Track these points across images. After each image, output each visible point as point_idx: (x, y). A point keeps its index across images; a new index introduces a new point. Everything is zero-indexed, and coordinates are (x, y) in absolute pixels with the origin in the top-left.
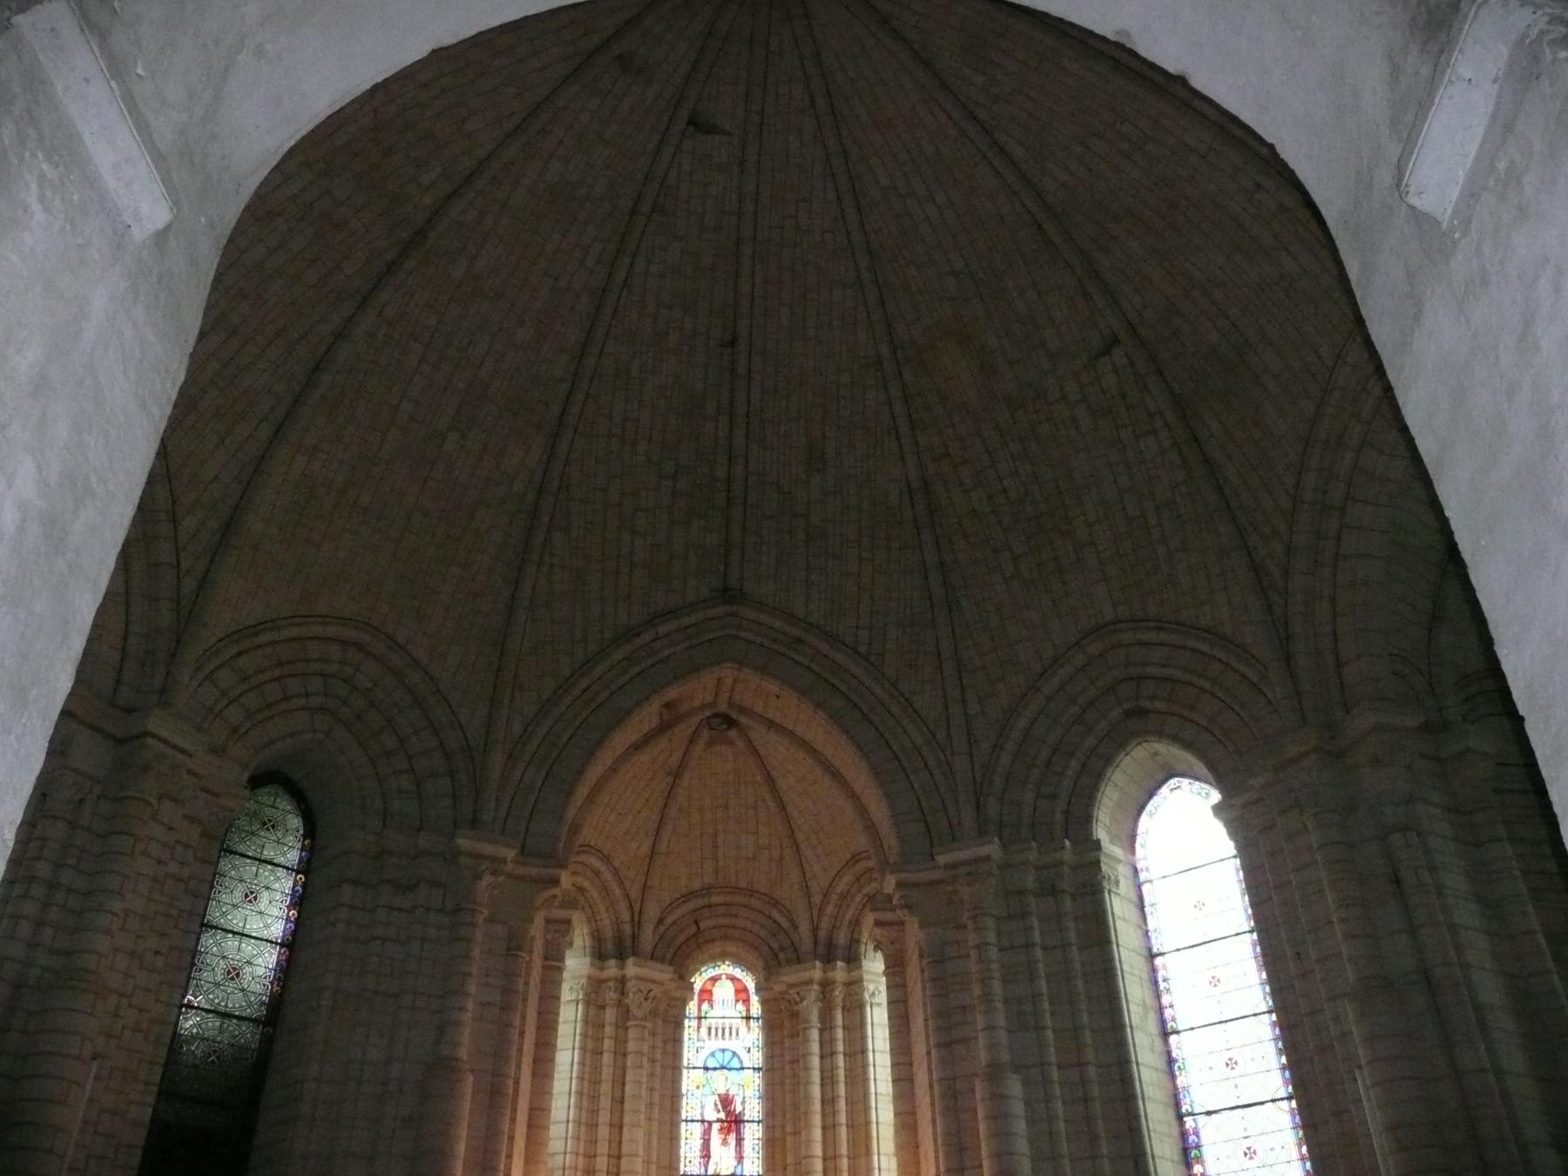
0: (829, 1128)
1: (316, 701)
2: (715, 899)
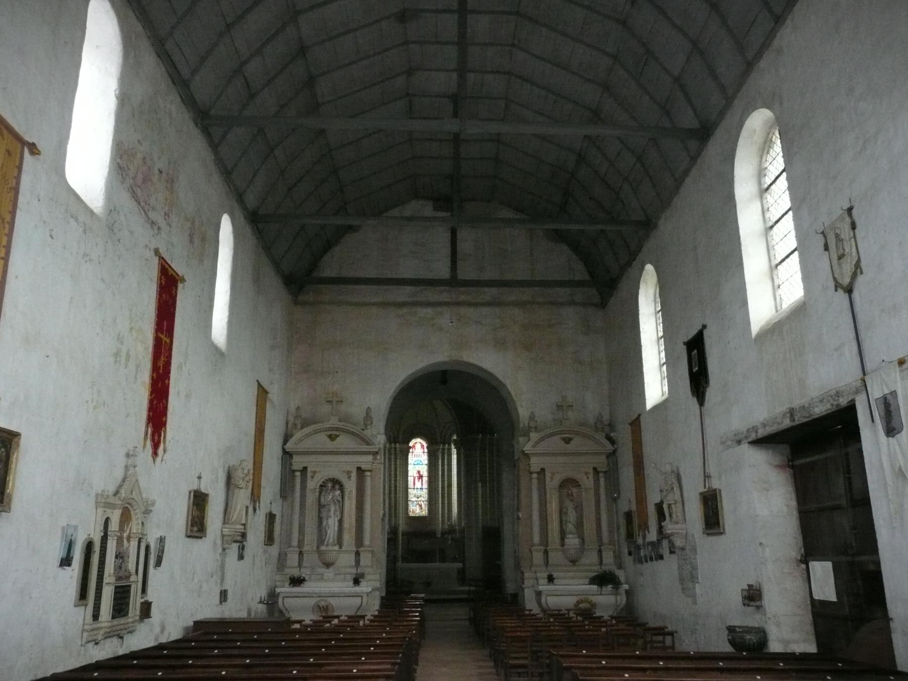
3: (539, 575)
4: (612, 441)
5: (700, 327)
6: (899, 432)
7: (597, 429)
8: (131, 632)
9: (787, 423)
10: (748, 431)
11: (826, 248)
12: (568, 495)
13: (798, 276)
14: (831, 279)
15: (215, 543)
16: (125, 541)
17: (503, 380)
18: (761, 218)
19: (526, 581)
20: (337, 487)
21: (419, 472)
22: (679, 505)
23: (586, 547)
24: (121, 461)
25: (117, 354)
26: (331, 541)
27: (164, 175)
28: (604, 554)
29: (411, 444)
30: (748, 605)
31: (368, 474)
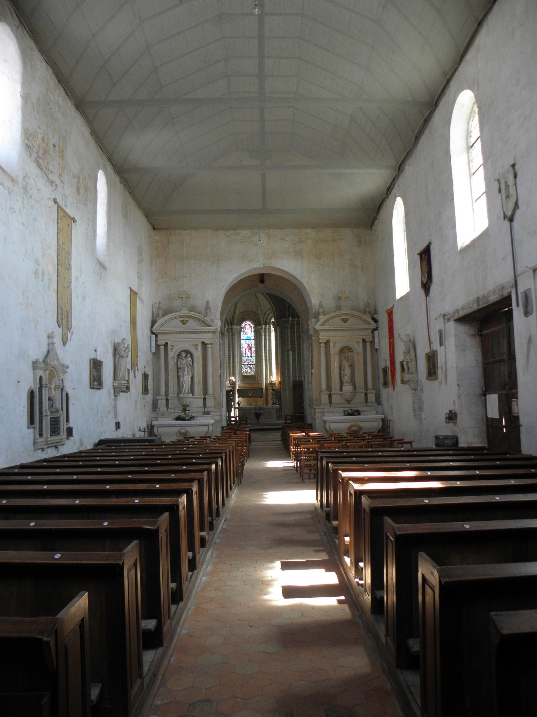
0: (266, 351)
3: (325, 410)
4: (376, 321)
5: (426, 244)
6: (531, 314)
7: (365, 313)
8: (63, 445)
9: (475, 307)
10: (454, 312)
11: (500, 191)
12: (345, 358)
13: (485, 208)
14: (502, 212)
15: (109, 392)
16: (53, 390)
17: (301, 280)
18: (467, 167)
19: (317, 414)
20: (189, 355)
21: (249, 345)
22: (414, 362)
23: (357, 391)
24: (45, 341)
25: (36, 273)
26: (186, 391)
27: (57, 147)
28: (369, 395)
29: (243, 325)
30: (449, 423)
31: (210, 346)
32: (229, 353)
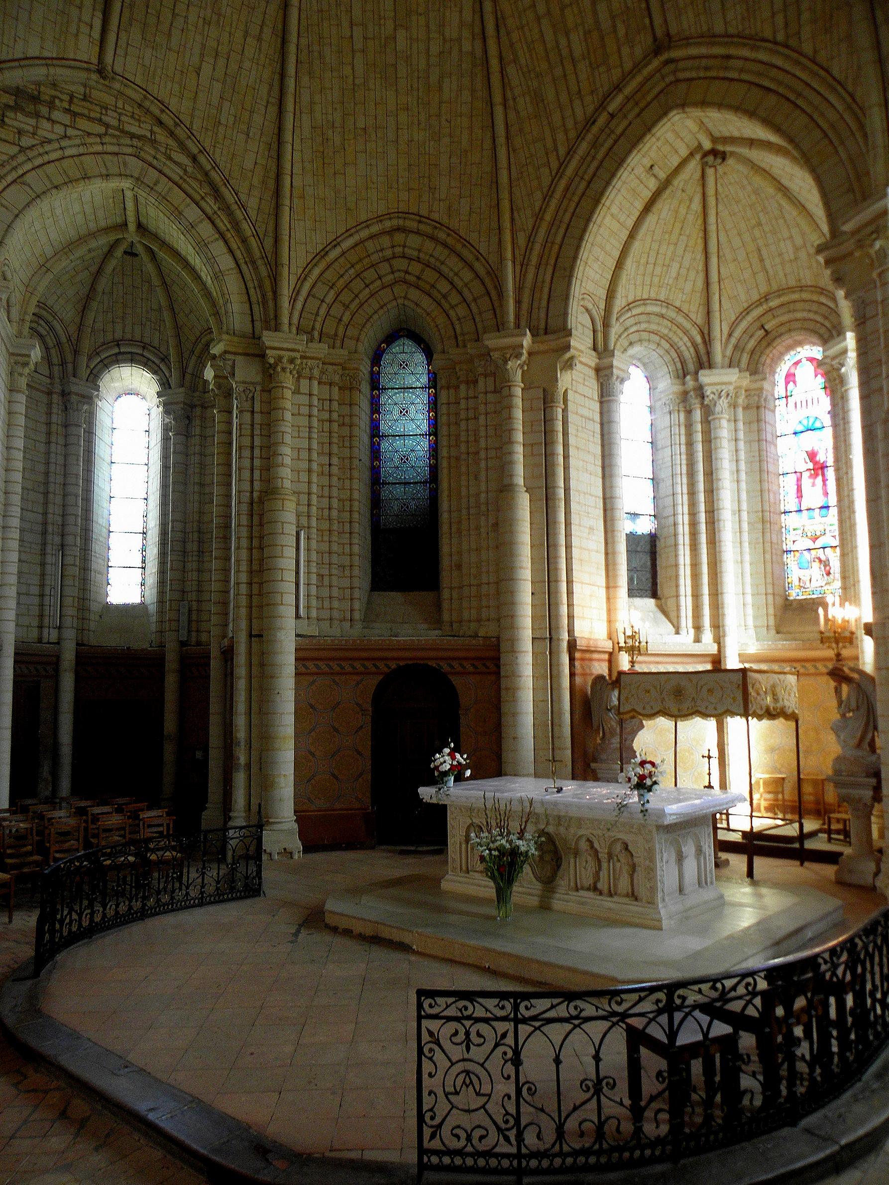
1: (389, 278)
2: (772, 304)
21: (812, 456)
32: (693, 504)
